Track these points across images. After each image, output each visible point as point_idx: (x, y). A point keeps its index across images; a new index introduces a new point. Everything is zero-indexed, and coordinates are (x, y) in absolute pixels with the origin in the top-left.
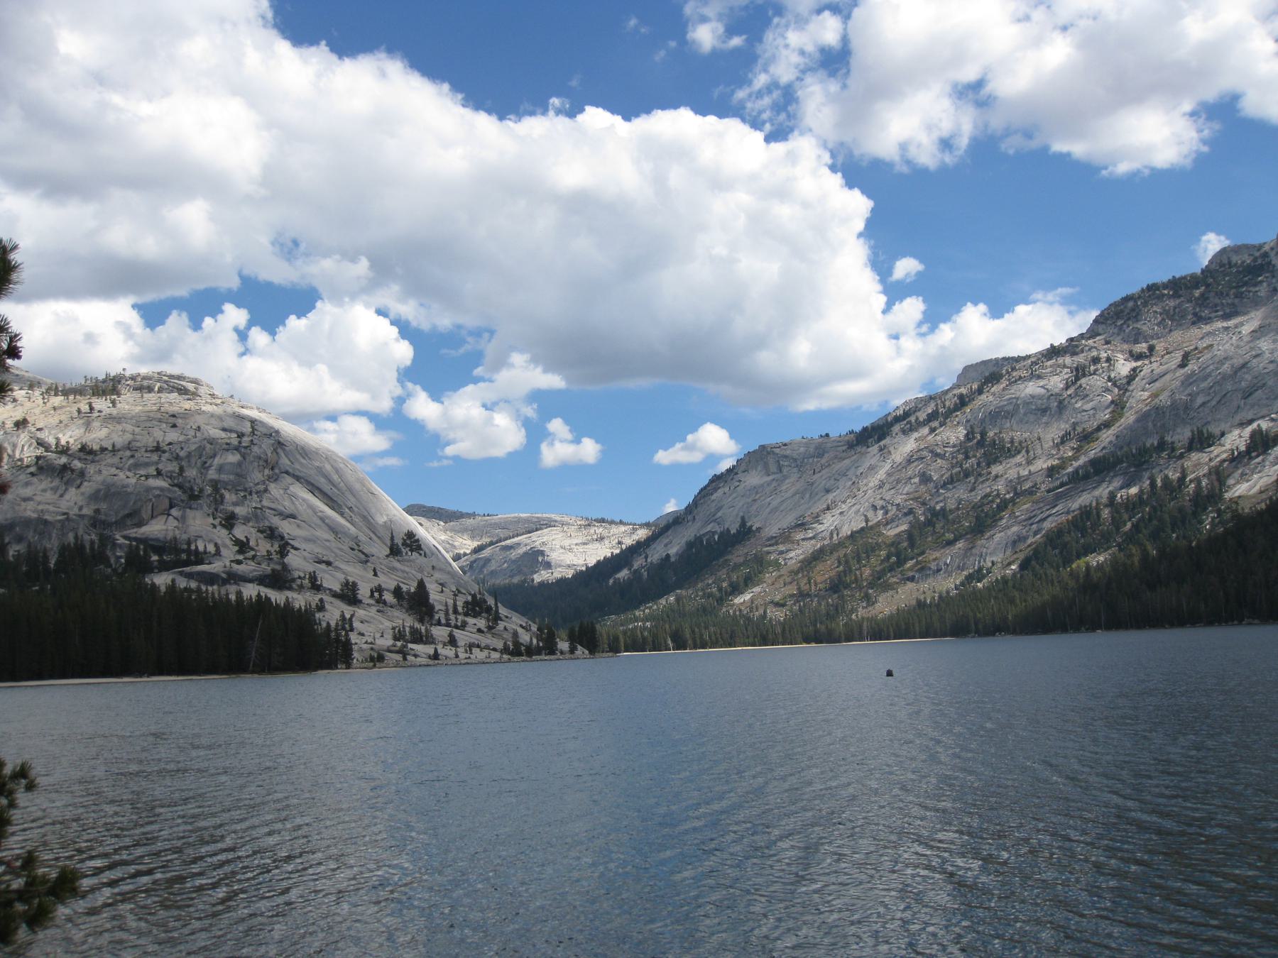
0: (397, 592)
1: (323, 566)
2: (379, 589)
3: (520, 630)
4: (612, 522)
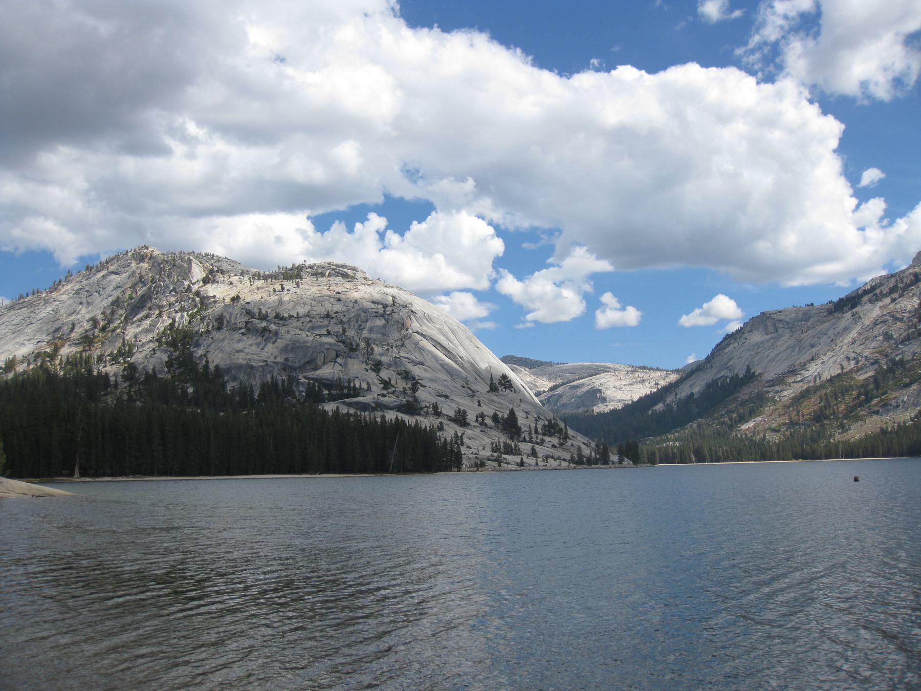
0: (495, 418)
1: (443, 399)
2: (482, 416)
3: (583, 446)
4: (651, 369)
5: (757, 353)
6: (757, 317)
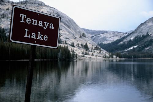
0: (82, 45)
1: (67, 39)
2: (78, 44)
3: (106, 53)
4: (119, 32)
5: (150, 29)
6: (151, 19)
